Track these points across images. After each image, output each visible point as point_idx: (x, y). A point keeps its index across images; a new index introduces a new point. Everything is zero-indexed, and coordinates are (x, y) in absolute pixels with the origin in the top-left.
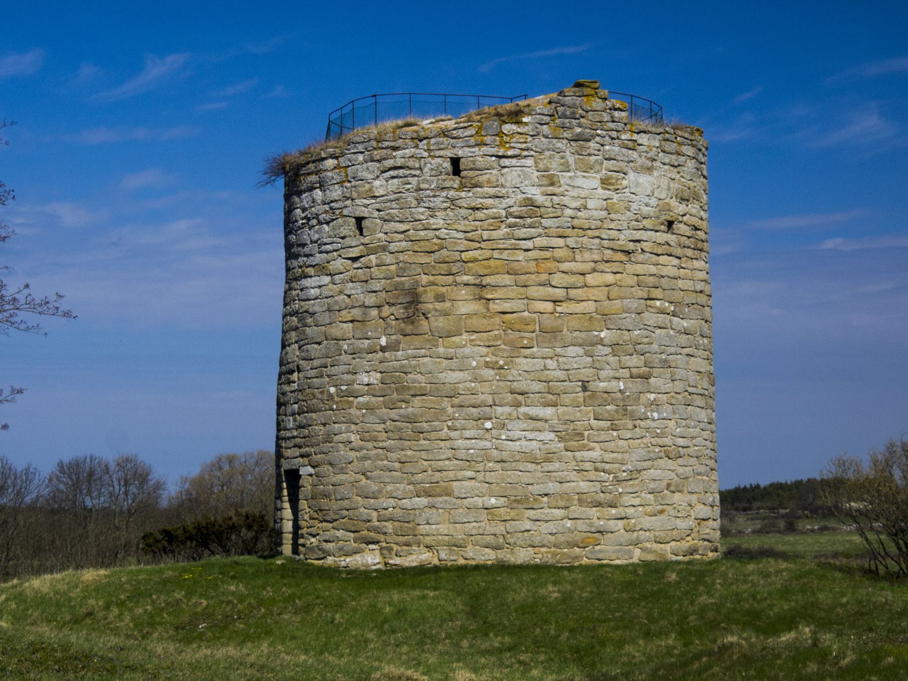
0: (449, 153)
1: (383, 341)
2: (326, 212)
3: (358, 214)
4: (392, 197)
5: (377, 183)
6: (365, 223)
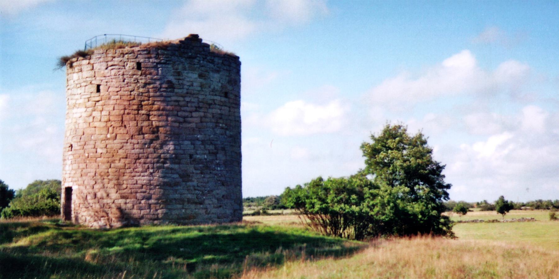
0: (137, 60)
1: (109, 136)
2: (84, 82)
3: (98, 83)
4: (113, 77)
5: (107, 71)
6: (101, 87)
